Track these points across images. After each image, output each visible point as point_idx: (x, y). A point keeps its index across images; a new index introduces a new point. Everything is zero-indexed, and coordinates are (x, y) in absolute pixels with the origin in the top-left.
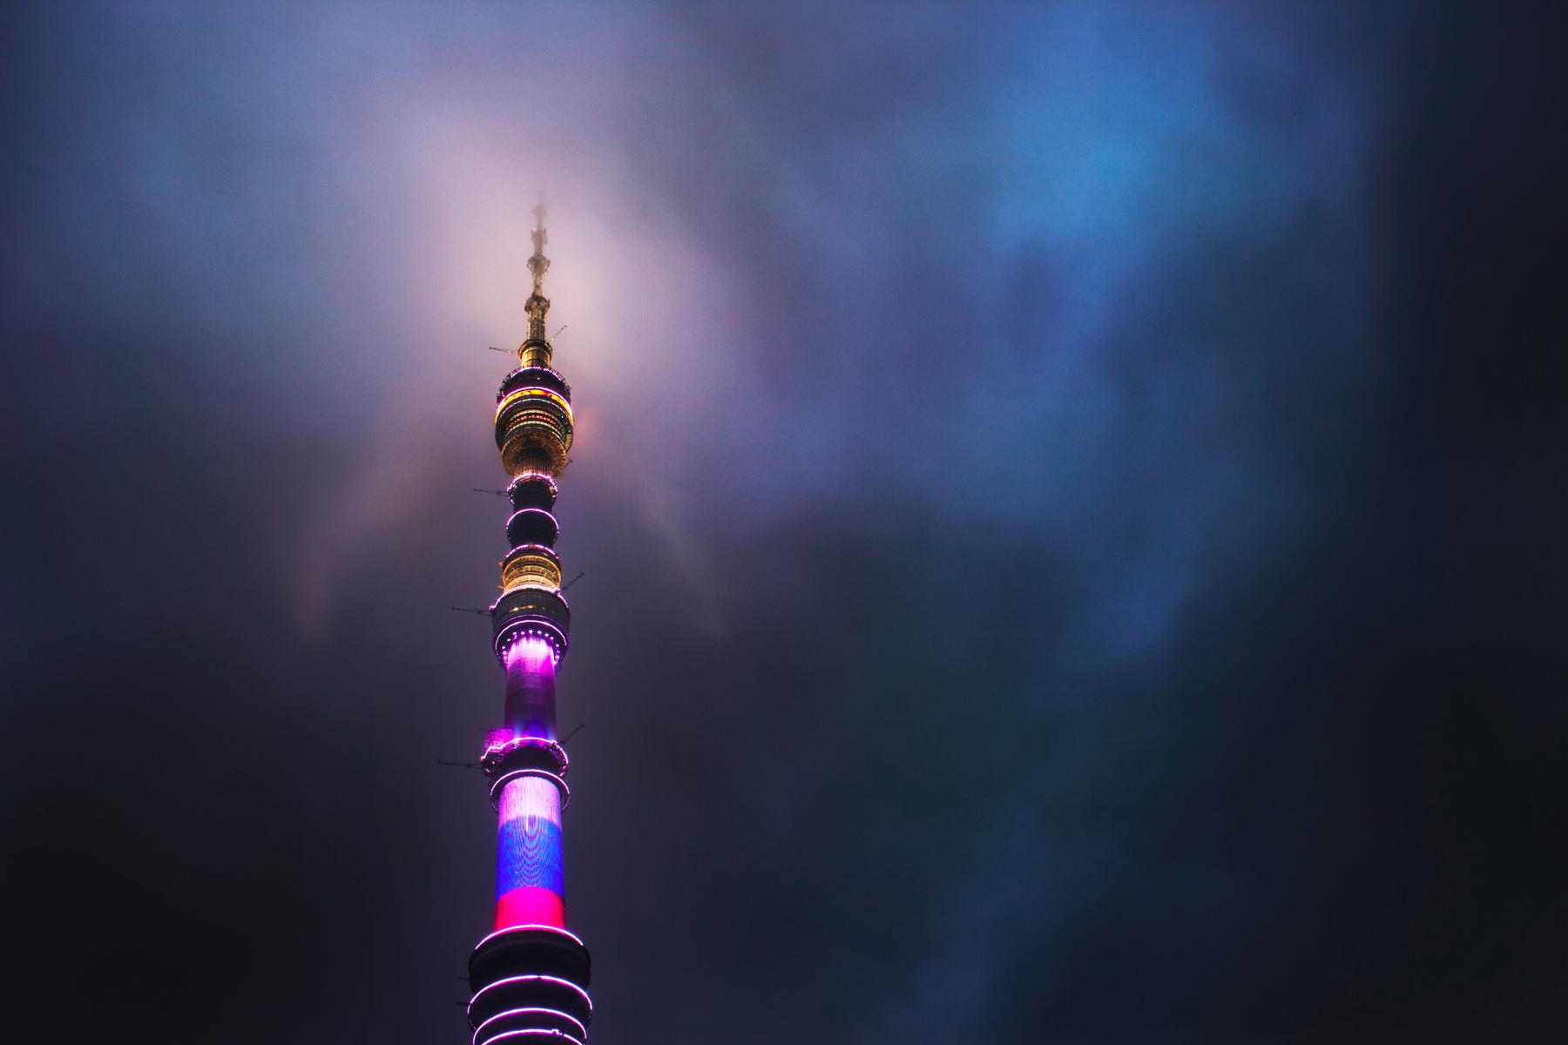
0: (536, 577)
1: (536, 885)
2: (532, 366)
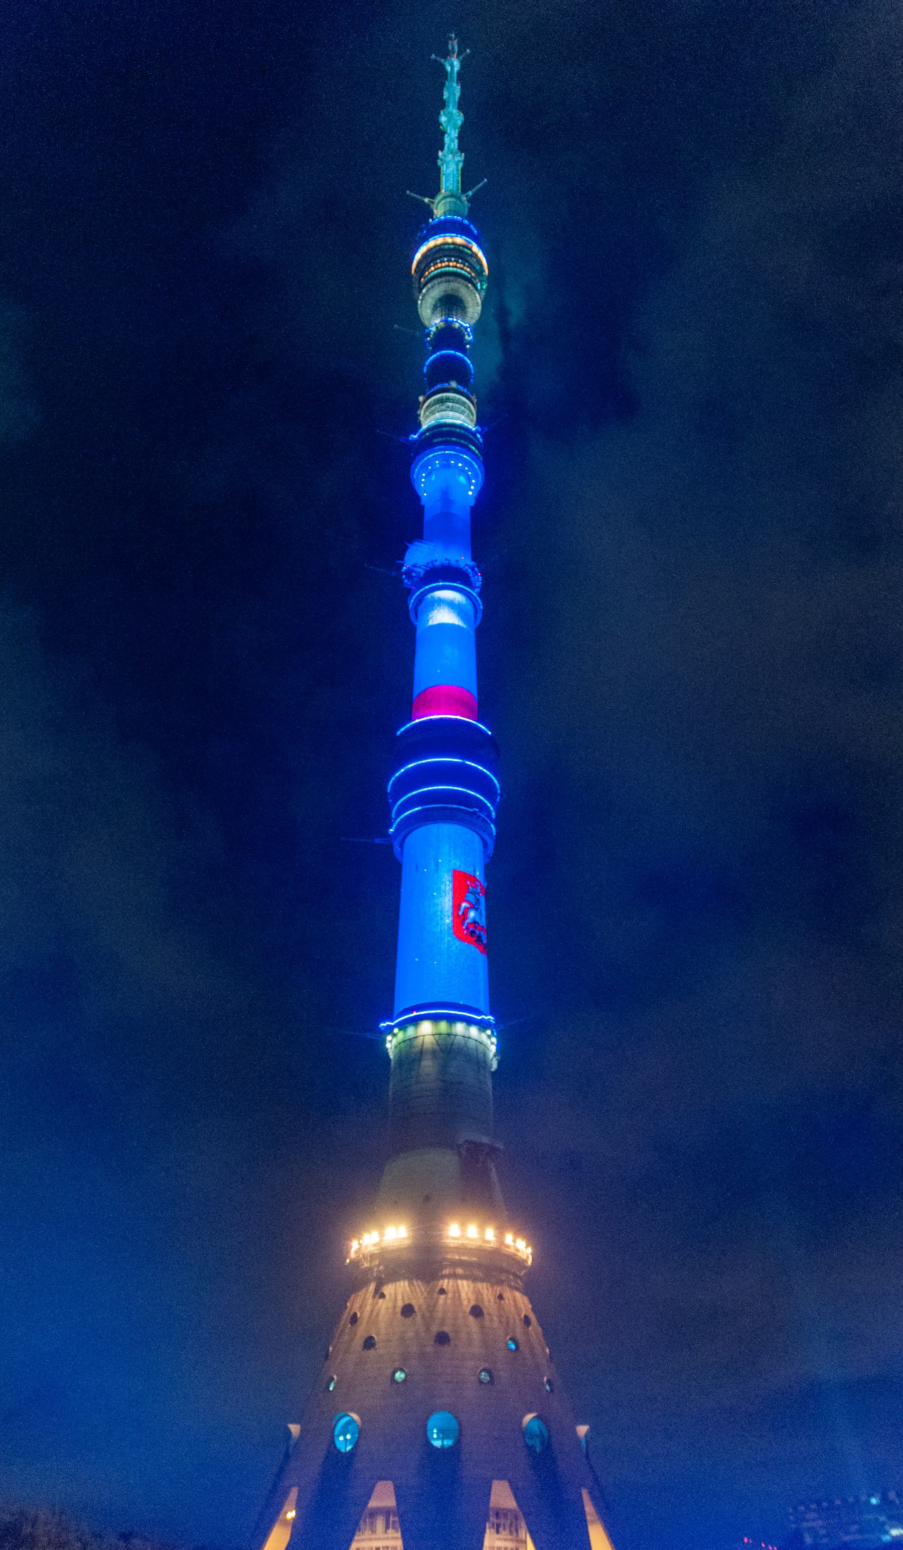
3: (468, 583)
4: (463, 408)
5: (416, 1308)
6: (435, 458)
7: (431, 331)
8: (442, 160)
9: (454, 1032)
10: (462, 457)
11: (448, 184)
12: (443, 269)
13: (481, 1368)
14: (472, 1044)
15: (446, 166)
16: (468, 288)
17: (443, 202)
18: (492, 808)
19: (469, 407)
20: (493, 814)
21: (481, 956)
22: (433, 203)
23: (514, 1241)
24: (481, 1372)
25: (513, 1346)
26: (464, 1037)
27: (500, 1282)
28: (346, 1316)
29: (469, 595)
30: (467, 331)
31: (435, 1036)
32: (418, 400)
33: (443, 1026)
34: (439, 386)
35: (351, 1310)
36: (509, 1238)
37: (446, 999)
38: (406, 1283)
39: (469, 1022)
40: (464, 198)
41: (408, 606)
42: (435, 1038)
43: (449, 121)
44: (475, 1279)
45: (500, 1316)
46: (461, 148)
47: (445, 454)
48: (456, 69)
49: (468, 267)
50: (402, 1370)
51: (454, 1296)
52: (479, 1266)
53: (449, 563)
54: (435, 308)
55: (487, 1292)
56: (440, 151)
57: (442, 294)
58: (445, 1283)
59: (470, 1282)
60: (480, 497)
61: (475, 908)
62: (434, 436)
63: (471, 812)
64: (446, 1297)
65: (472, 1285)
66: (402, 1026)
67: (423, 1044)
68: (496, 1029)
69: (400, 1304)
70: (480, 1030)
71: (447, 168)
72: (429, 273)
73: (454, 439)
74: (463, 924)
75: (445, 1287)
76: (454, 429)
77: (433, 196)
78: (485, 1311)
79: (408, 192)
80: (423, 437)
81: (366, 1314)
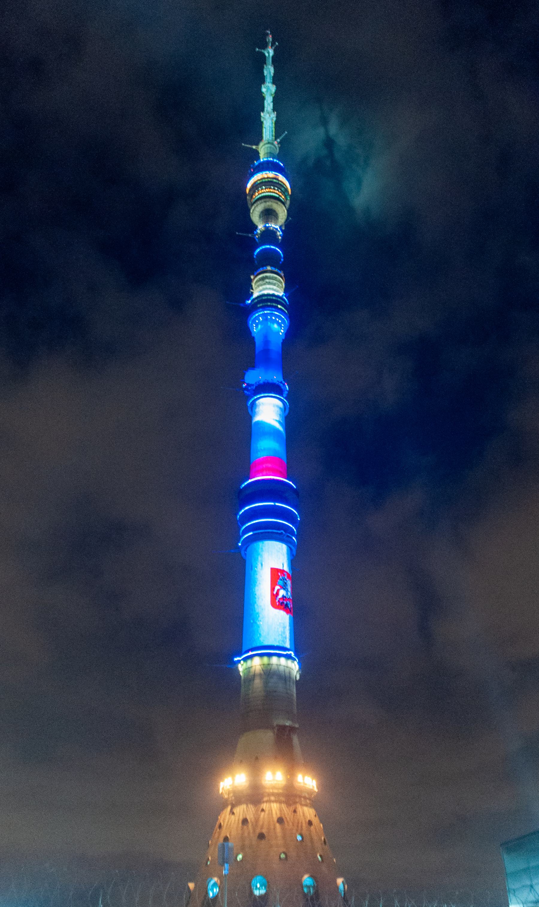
0: (271, 286)
1: (269, 268)
2: (267, 158)
5: (249, 820)
6: (259, 316)
8: (263, 118)
9: (271, 663)
14: (281, 668)
15: (266, 122)
17: (264, 147)
22: (258, 148)
23: (303, 779)
26: (277, 665)
28: (217, 826)
32: (250, 278)
33: (265, 659)
38: (245, 806)
39: (279, 655)
40: (275, 143)
42: (261, 667)
43: (267, 91)
44: (280, 802)
60: (288, 334)
61: (283, 588)
62: (259, 302)
64: (264, 814)
66: (245, 659)
67: (255, 671)
69: (241, 818)
72: (256, 196)
73: (269, 304)
74: (276, 599)
75: (264, 808)
76: (269, 297)
77: (257, 144)
79: (243, 144)
81: (226, 823)
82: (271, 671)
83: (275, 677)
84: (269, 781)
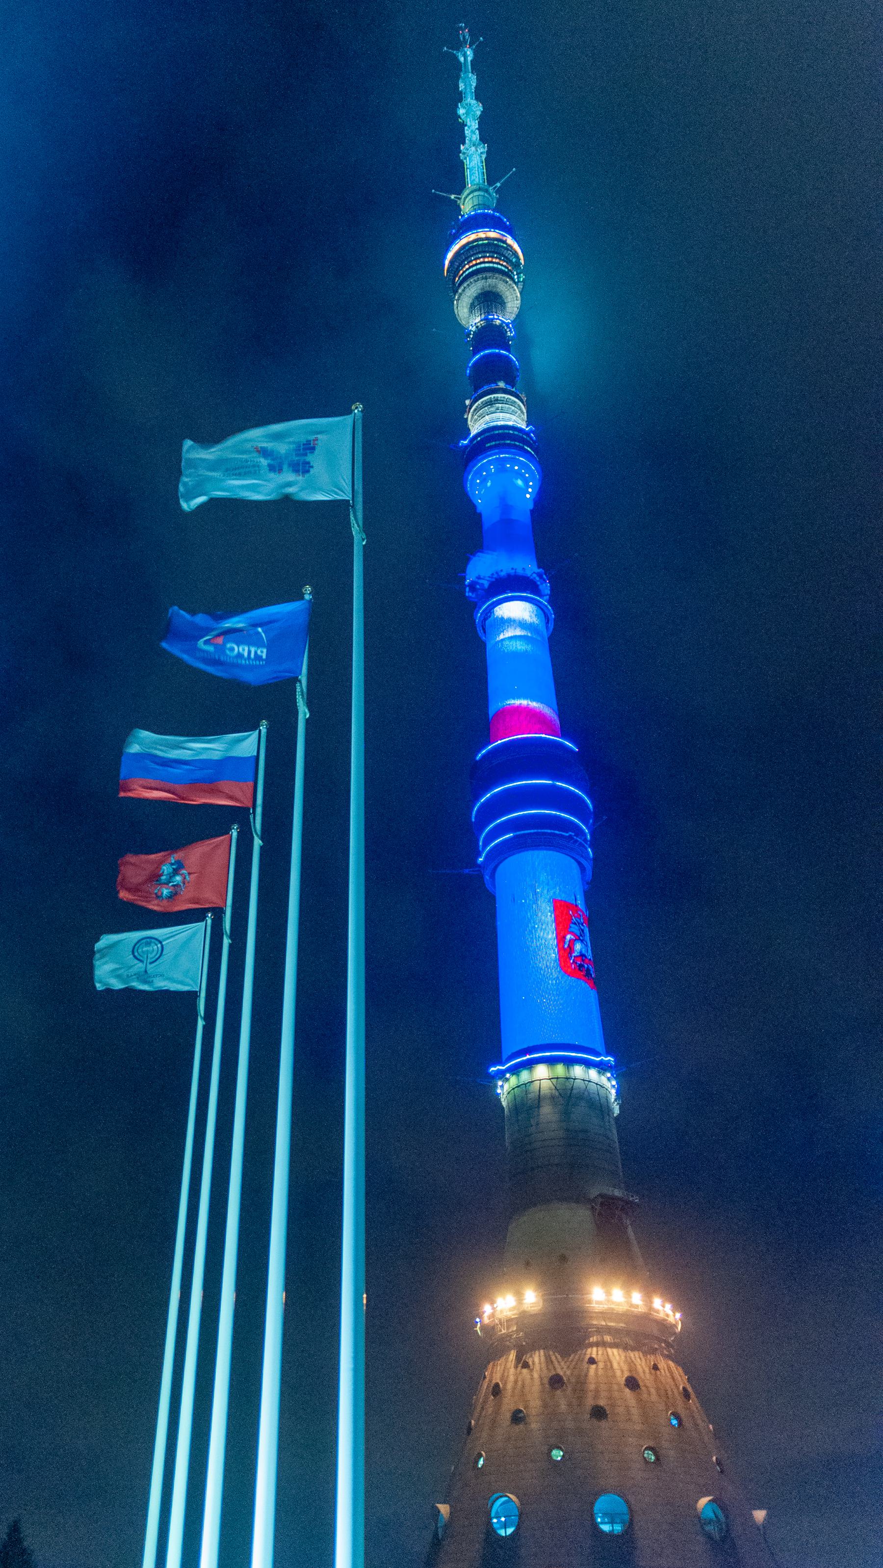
3: (537, 592)
4: (513, 408)
7: (471, 331)
8: (464, 153)
10: (519, 460)
11: (473, 178)
12: (479, 267)
13: (644, 1448)
14: (592, 1087)
16: (507, 282)
18: (587, 831)
19: (519, 406)
20: (589, 837)
21: (592, 991)
24: (644, 1451)
25: (674, 1422)
27: (653, 1351)
29: (538, 604)
30: (509, 327)
31: (552, 1080)
33: (560, 1069)
34: (486, 388)
35: (490, 1381)
36: (657, 1302)
37: (559, 1040)
39: (588, 1064)
41: (475, 620)
43: (467, 113)
44: (626, 1348)
45: (658, 1389)
46: (483, 139)
47: (500, 457)
48: (469, 59)
49: (504, 261)
50: (559, 1448)
51: (606, 1365)
52: (628, 1333)
53: (515, 572)
54: (472, 307)
55: (641, 1364)
56: (461, 145)
57: (479, 291)
58: (593, 1352)
59: (621, 1351)
60: (539, 500)
61: (580, 939)
63: (566, 836)
65: (623, 1355)
66: (515, 1070)
68: (616, 1071)
70: (599, 1073)
71: (471, 161)
75: (594, 1356)
77: (460, 192)
78: (641, 1384)
80: (475, 442)
82: (574, 1091)
83: (583, 1104)
84: (598, 1303)
